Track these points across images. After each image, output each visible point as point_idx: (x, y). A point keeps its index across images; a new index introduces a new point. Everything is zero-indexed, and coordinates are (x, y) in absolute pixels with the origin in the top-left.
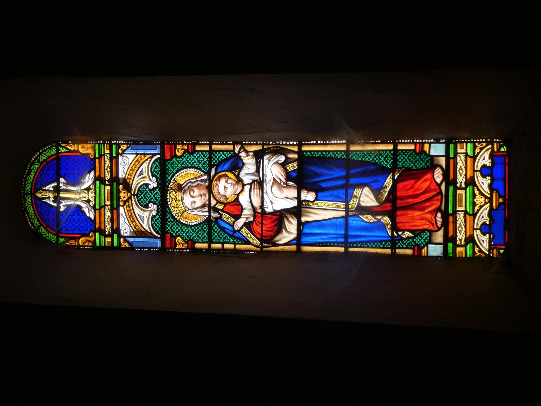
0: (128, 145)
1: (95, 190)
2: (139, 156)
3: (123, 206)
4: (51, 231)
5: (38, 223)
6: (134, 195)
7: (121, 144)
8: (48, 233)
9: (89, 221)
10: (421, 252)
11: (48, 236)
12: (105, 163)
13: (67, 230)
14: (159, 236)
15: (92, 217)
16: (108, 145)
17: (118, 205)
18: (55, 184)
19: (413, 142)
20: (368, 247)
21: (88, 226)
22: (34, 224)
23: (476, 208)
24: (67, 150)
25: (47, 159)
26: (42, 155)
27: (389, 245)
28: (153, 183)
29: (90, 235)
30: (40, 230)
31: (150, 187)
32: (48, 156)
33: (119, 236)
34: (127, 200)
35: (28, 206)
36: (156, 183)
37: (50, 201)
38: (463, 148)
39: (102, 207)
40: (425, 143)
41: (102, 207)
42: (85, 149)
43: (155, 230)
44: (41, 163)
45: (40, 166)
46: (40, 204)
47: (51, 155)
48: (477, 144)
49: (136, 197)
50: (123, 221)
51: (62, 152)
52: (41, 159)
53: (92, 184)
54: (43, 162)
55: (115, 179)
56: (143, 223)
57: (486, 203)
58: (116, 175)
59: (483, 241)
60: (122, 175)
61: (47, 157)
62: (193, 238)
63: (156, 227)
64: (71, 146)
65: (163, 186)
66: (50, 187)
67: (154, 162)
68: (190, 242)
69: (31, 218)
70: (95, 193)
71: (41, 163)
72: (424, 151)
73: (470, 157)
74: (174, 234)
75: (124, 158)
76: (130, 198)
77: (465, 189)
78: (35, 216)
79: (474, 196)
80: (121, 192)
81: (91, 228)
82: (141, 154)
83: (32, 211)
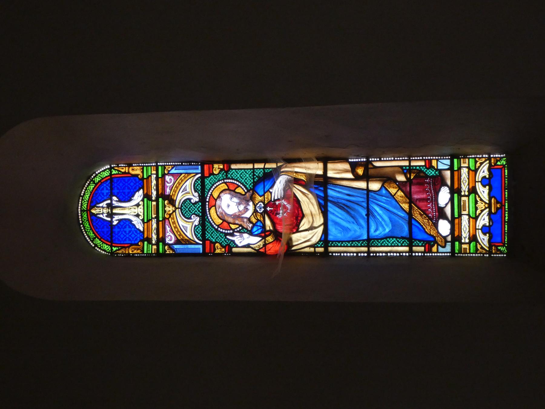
0: (173, 166)
1: (144, 206)
4: (105, 242)
5: (93, 235)
6: (178, 208)
8: (103, 243)
9: (138, 232)
11: (102, 247)
13: (119, 240)
14: (201, 243)
15: (142, 229)
16: (155, 167)
18: (109, 202)
19: (423, 159)
20: (347, 246)
21: (115, 237)
22: (90, 236)
23: (478, 212)
24: (119, 173)
25: (101, 180)
26: (97, 177)
27: (366, 243)
28: (195, 198)
29: (139, 244)
30: (95, 241)
31: (192, 201)
33: (165, 244)
35: (84, 221)
36: (198, 197)
37: (104, 216)
38: (466, 163)
40: (433, 159)
41: (150, 220)
45: (95, 186)
46: (94, 219)
47: (105, 176)
48: (477, 159)
49: (180, 209)
51: (114, 174)
52: (96, 180)
53: (141, 201)
54: (98, 183)
55: (163, 195)
56: (187, 232)
57: (486, 208)
61: (101, 179)
62: (222, 243)
63: (197, 234)
66: (104, 204)
67: (196, 181)
68: (227, 247)
69: (87, 231)
71: (96, 184)
72: (433, 166)
76: (174, 211)
77: (468, 196)
78: (90, 229)
79: (476, 202)
83: (88, 225)
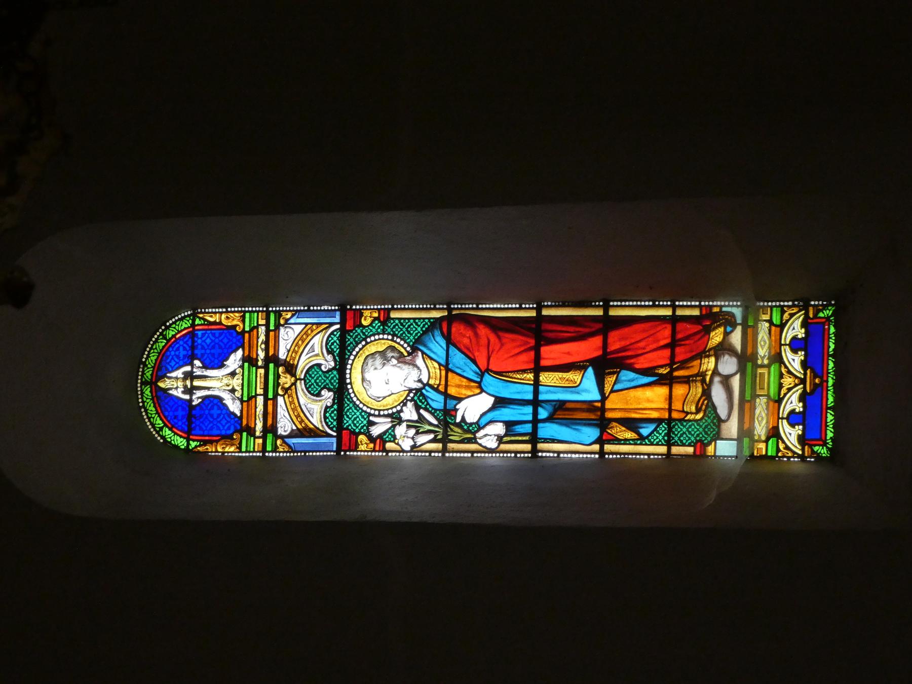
1: (243, 375)
2: (309, 326)
3: (283, 396)
7: (283, 311)
9: (232, 417)
10: (705, 451)
11: (174, 440)
12: (258, 338)
17: (276, 395)
22: (155, 424)
23: (783, 391)
25: (176, 334)
31: (323, 368)
32: (178, 331)
33: (276, 437)
34: (290, 388)
37: (178, 393)
38: (767, 314)
39: (252, 398)
41: (253, 397)
42: (230, 318)
43: (328, 426)
44: (168, 341)
46: (162, 398)
48: (785, 309)
50: (282, 411)
52: (169, 334)
54: (171, 339)
55: (272, 359)
56: (313, 417)
57: (796, 385)
58: (273, 353)
59: (794, 329)
60: (282, 355)
64: (211, 316)
65: (341, 367)
66: (179, 373)
67: (329, 336)
70: (243, 379)
73: (776, 326)
74: (357, 430)
75: (287, 330)
76: (294, 384)
79: (781, 376)
80: (281, 377)
81: (235, 427)
82: (313, 324)
